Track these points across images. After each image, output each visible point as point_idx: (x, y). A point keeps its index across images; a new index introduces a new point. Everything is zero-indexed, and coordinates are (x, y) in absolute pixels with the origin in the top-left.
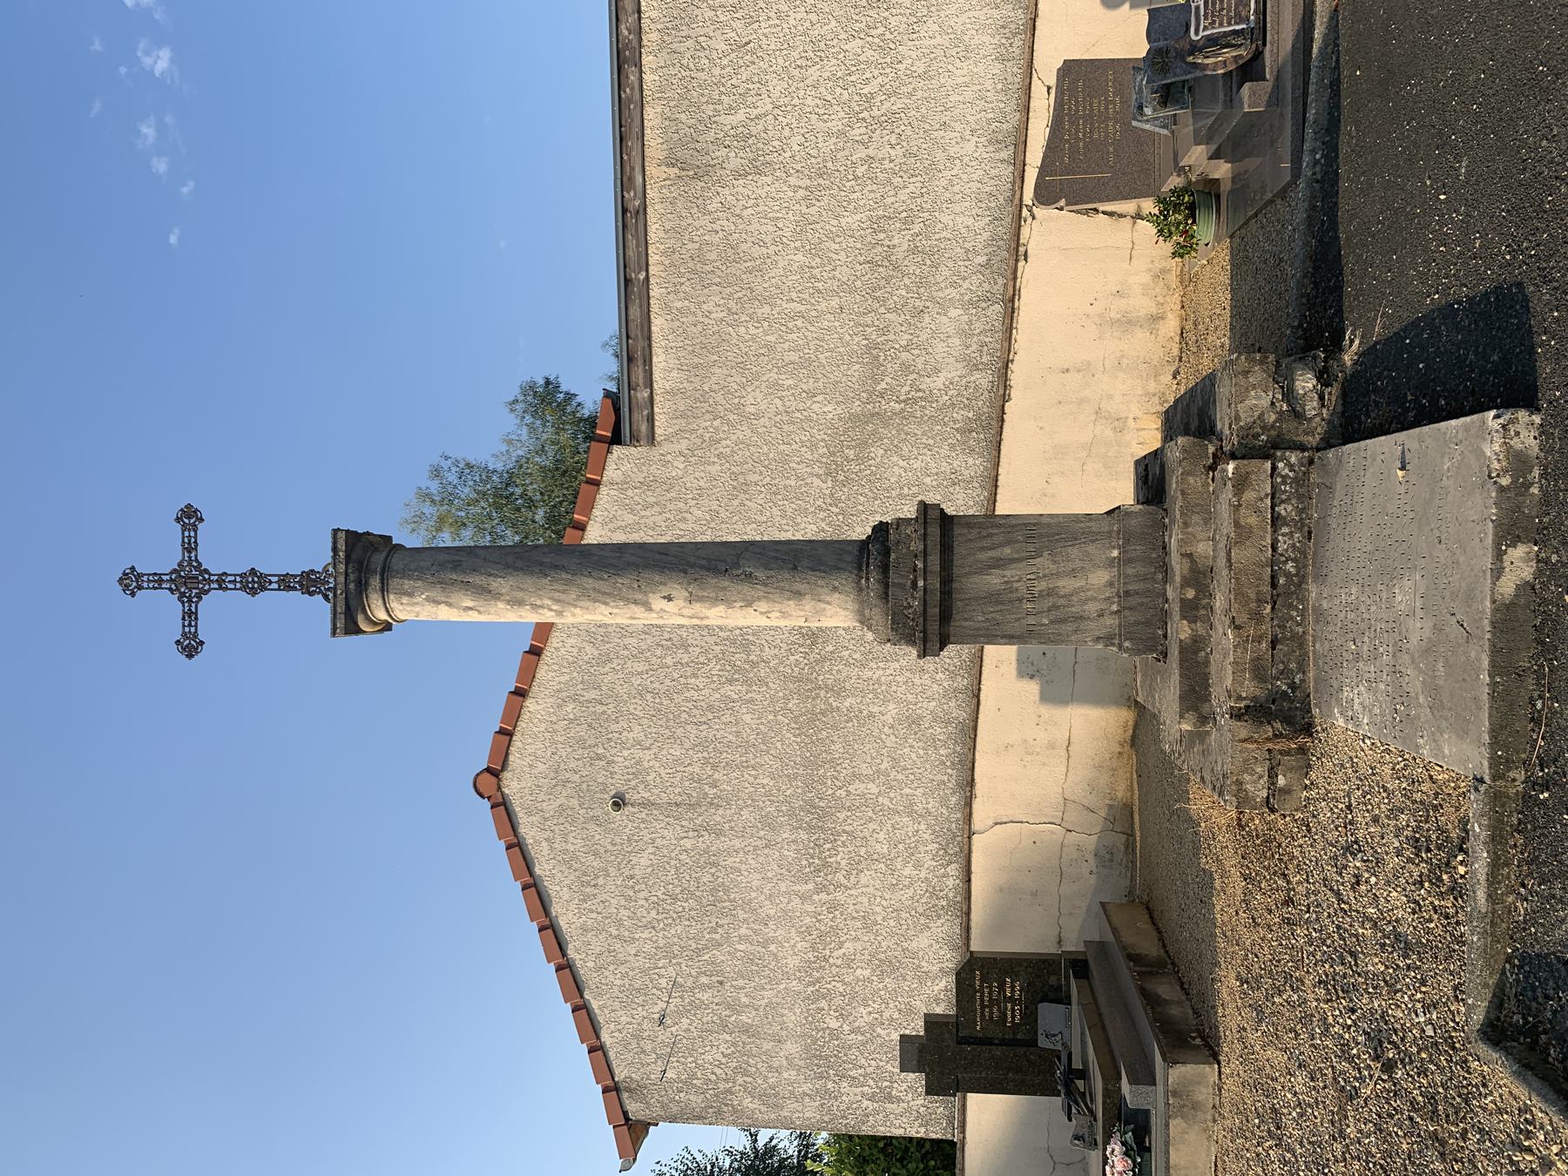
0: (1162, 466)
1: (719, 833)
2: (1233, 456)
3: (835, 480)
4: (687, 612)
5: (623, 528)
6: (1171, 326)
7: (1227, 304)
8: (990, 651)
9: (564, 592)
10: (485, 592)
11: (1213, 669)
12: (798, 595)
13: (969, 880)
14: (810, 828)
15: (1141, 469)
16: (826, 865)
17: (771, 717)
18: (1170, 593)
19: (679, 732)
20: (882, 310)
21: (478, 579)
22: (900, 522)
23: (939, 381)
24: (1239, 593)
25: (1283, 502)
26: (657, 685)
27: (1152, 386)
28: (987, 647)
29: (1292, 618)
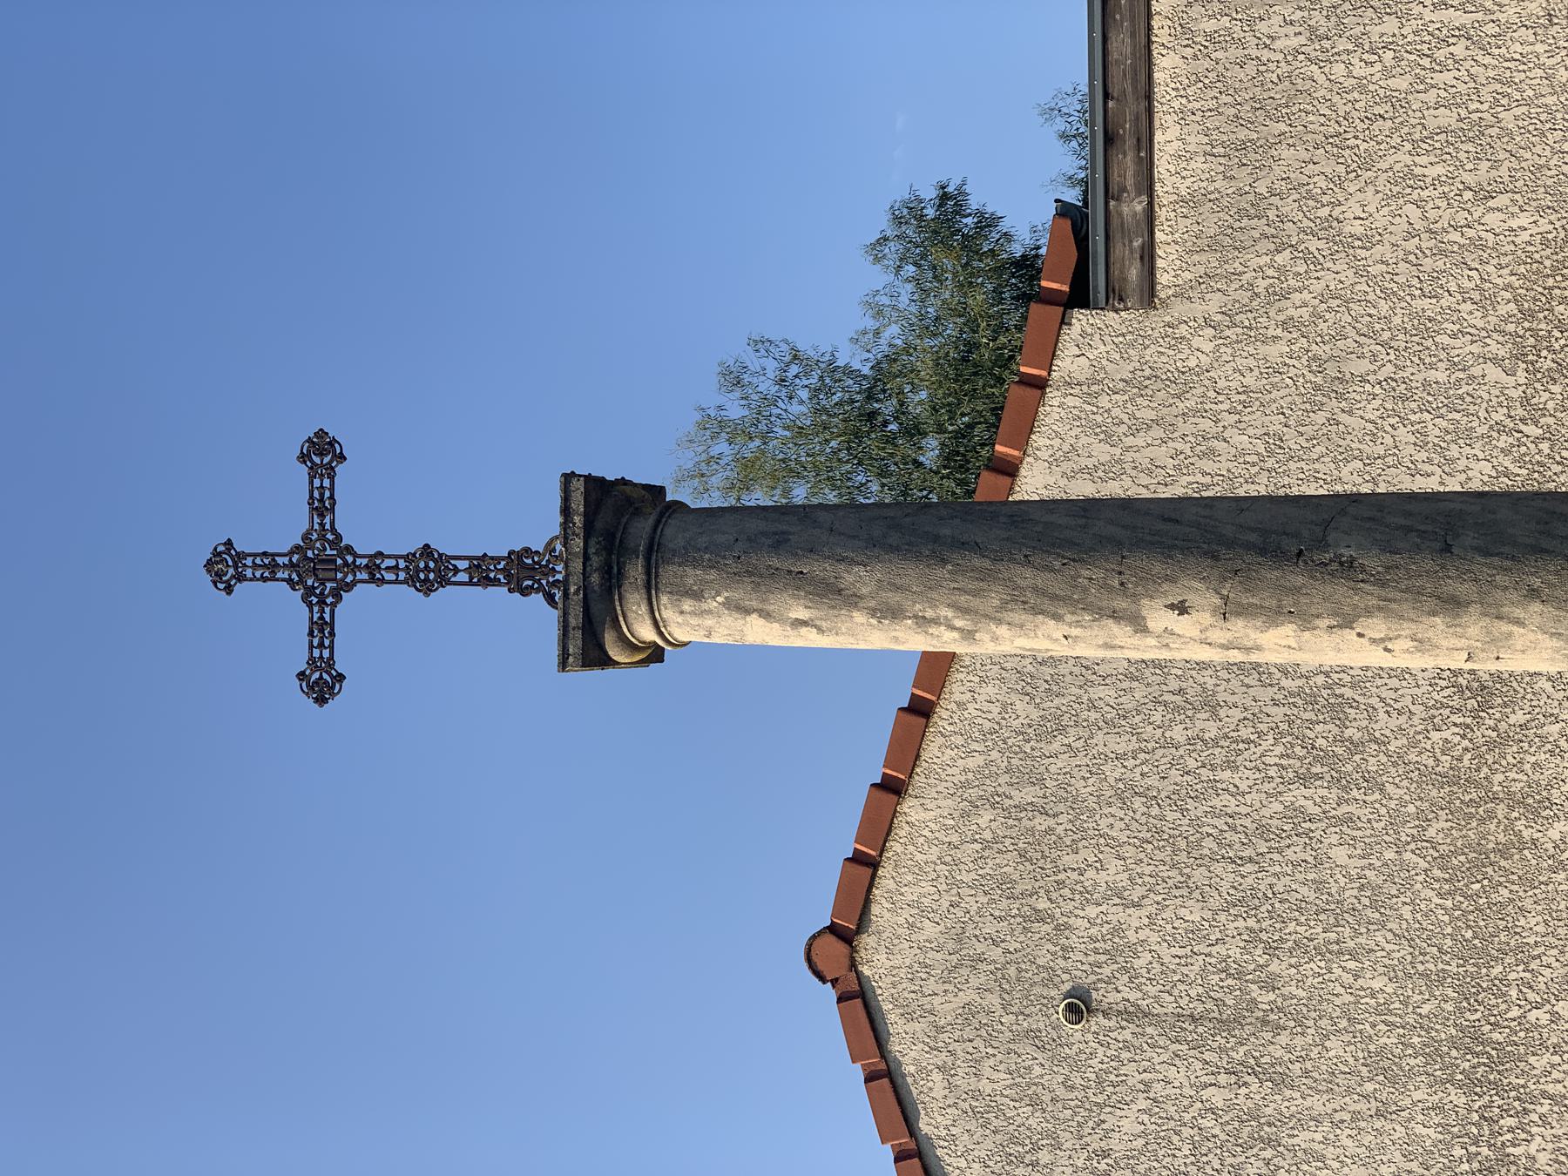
9: (975, 594)
10: (832, 594)
21: (817, 568)
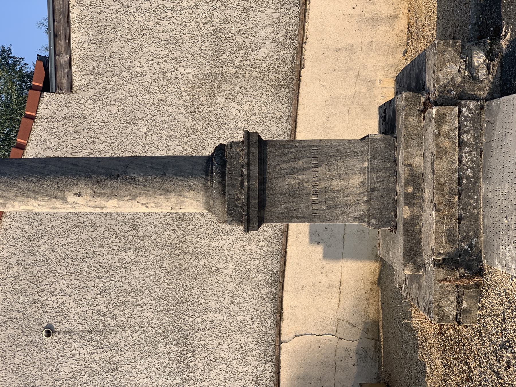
0: (394, 111)
1: (118, 349)
2: (436, 104)
3: (193, 118)
4: (92, 203)
5: (51, 148)
6: (402, 23)
7: (435, 9)
8: (293, 226)
9: (6, 191)
11: (424, 236)
12: (166, 192)
13: (279, 373)
14: (178, 344)
15: (382, 112)
16: (188, 367)
17: (152, 272)
18: (398, 190)
19: (91, 283)
20: (223, 8)
22: (232, 144)
23: (260, 55)
24: (439, 189)
25: (465, 132)
26: (75, 253)
27: (390, 61)
28: (290, 224)
29: (470, 204)
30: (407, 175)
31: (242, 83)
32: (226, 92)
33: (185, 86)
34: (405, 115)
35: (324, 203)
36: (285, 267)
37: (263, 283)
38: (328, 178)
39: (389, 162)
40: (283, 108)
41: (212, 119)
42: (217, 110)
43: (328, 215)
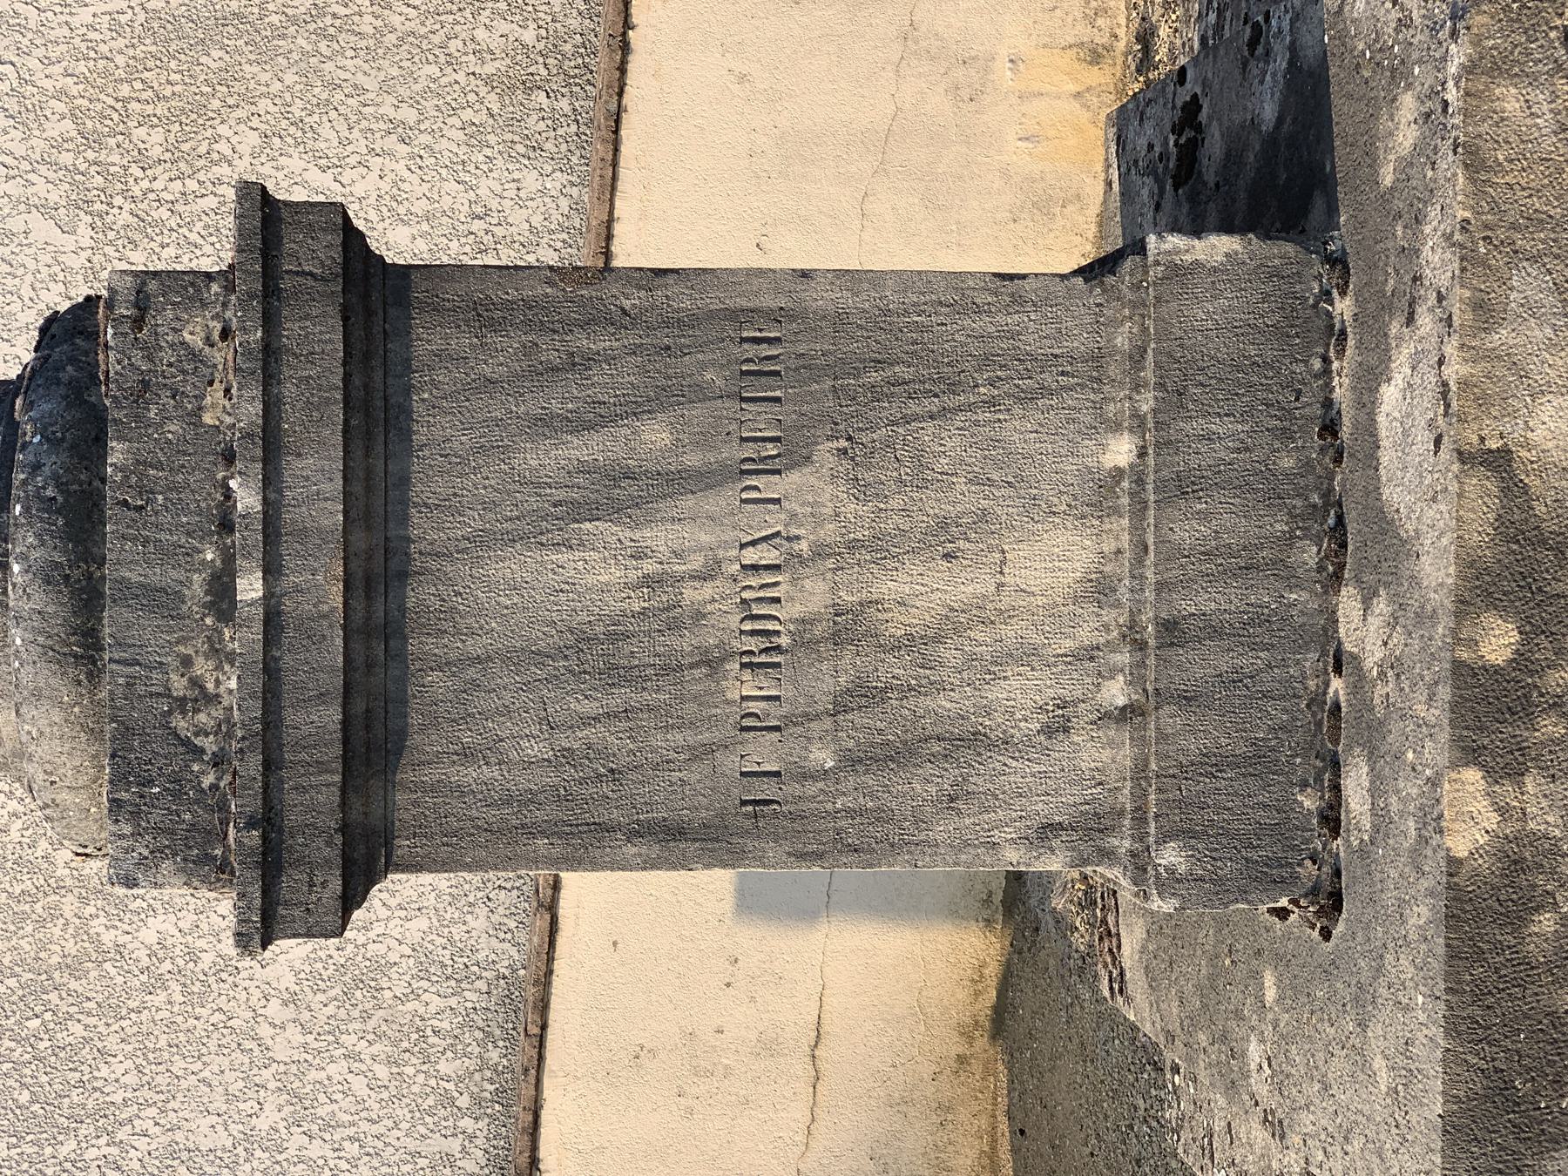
3: (100, 226)
22: (148, 294)
30: (1480, 531)
31: (341, 62)
32: (264, 105)
33: (57, 69)
34: (1469, 69)
35: (828, 723)
36: (550, 959)
37: (446, 1025)
38: (853, 546)
39: (1285, 435)
40: (543, 192)
41: (193, 237)
42: (221, 190)
43: (851, 813)
